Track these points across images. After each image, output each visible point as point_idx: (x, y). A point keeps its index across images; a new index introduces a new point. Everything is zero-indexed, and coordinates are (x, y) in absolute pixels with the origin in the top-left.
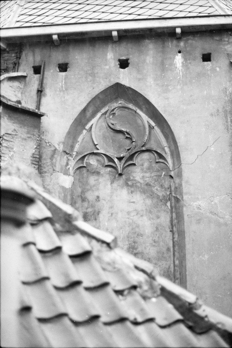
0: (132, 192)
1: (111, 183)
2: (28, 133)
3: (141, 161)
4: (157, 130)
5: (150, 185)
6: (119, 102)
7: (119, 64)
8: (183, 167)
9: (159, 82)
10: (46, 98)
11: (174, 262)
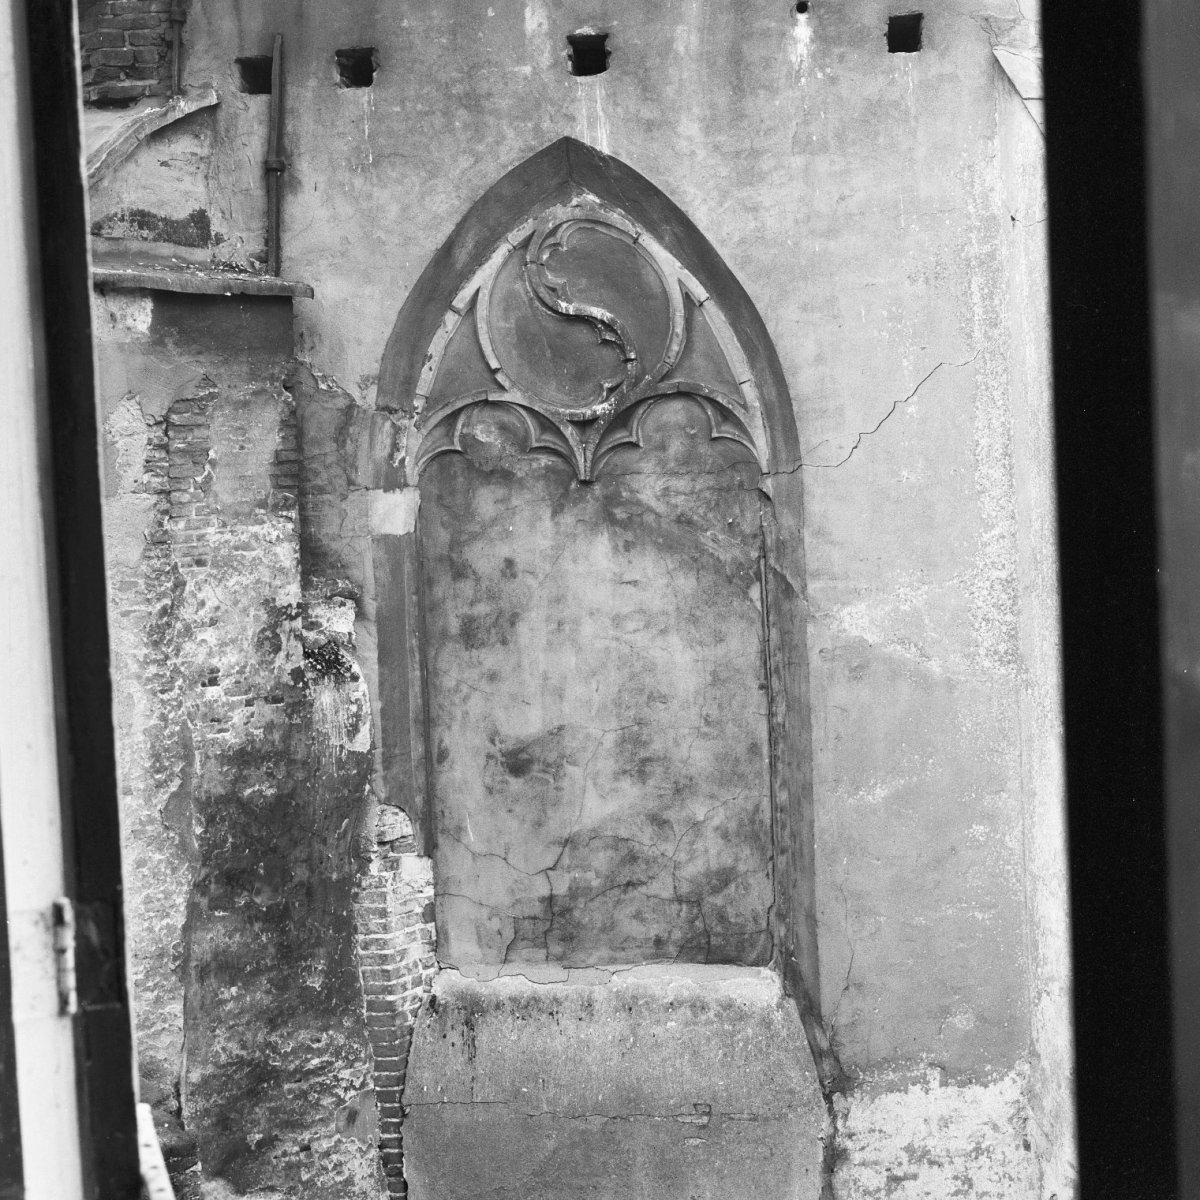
0: (628, 546)
1: (555, 513)
2: (253, 376)
3: (658, 429)
4: (714, 316)
5: (690, 522)
6: (575, 201)
7: (569, 56)
8: (808, 474)
9: (722, 138)
10: (300, 197)
11: (772, 796)
